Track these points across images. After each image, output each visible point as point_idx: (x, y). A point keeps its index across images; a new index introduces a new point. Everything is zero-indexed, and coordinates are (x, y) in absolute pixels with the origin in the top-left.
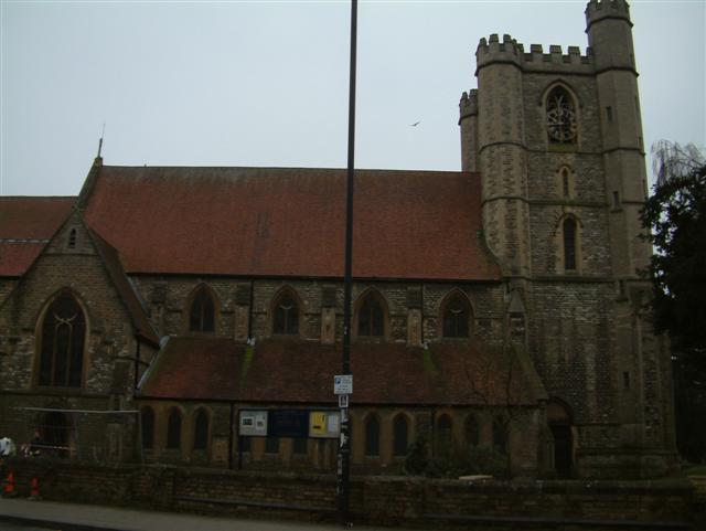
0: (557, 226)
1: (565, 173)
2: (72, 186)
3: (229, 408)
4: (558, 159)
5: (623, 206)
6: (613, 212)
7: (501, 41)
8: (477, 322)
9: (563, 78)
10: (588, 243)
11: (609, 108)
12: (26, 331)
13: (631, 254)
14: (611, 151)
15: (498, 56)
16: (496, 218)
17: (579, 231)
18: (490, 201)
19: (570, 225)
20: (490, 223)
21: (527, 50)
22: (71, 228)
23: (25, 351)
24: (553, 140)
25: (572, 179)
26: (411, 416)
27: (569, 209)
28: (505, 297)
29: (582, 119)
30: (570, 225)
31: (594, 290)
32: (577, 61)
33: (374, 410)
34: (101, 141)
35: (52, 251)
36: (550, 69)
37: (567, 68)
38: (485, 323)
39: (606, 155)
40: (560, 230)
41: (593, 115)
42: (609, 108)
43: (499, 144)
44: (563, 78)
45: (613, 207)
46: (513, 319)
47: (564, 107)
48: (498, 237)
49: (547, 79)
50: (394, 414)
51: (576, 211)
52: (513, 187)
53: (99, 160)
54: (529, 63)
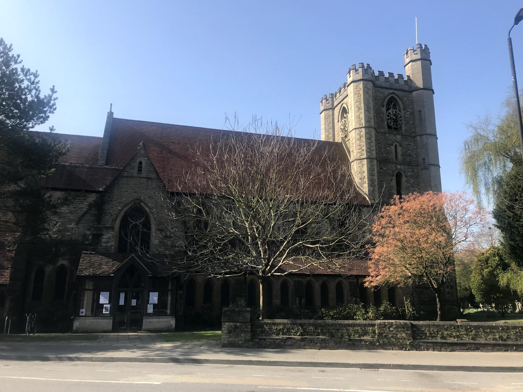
1: (396, 146)
2: (97, 130)
4: (392, 137)
9: (395, 92)
10: (409, 186)
12: (107, 228)
21: (377, 74)
22: (138, 161)
23: (108, 242)
24: (389, 127)
25: (399, 149)
27: (399, 167)
29: (405, 116)
32: (382, 79)
34: (111, 104)
35: (126, 174)
36: (388, 86)
37: (396, 86)
41: (410, 114)
44: (395, 92)
47: (394, 108)
49: (387, 92)
52: (373, 152)
53: (111, 114)
54: (377, 81)
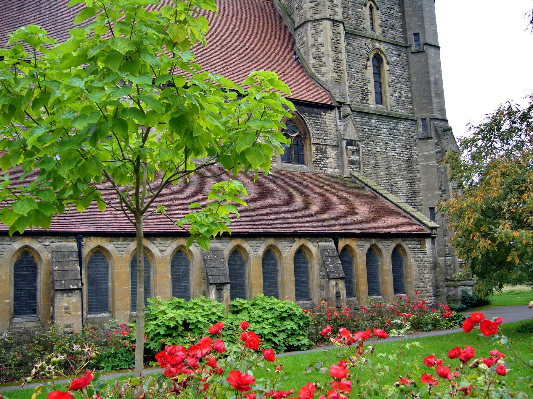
0: (368, 60)
3: (332, 244)
5: (425, 48)
8: (313, 148)
13: (433, 95)
16: (320, 40)
17: (386, 67)
18: (314, 21)
19: (378, 59)
20: (313, 45)
25: (377, 14)
26: (313, 247)
27: (377, 45)
28: (339, 123)
30: (378, 59)
31: (401, 126)
33: (271, 241)
38: (321, 150)
40: (370, 63)
45: (414, 48)
46: (349, 147)
48: (324, 60)
50: (296, 245)
51: (383, 47)
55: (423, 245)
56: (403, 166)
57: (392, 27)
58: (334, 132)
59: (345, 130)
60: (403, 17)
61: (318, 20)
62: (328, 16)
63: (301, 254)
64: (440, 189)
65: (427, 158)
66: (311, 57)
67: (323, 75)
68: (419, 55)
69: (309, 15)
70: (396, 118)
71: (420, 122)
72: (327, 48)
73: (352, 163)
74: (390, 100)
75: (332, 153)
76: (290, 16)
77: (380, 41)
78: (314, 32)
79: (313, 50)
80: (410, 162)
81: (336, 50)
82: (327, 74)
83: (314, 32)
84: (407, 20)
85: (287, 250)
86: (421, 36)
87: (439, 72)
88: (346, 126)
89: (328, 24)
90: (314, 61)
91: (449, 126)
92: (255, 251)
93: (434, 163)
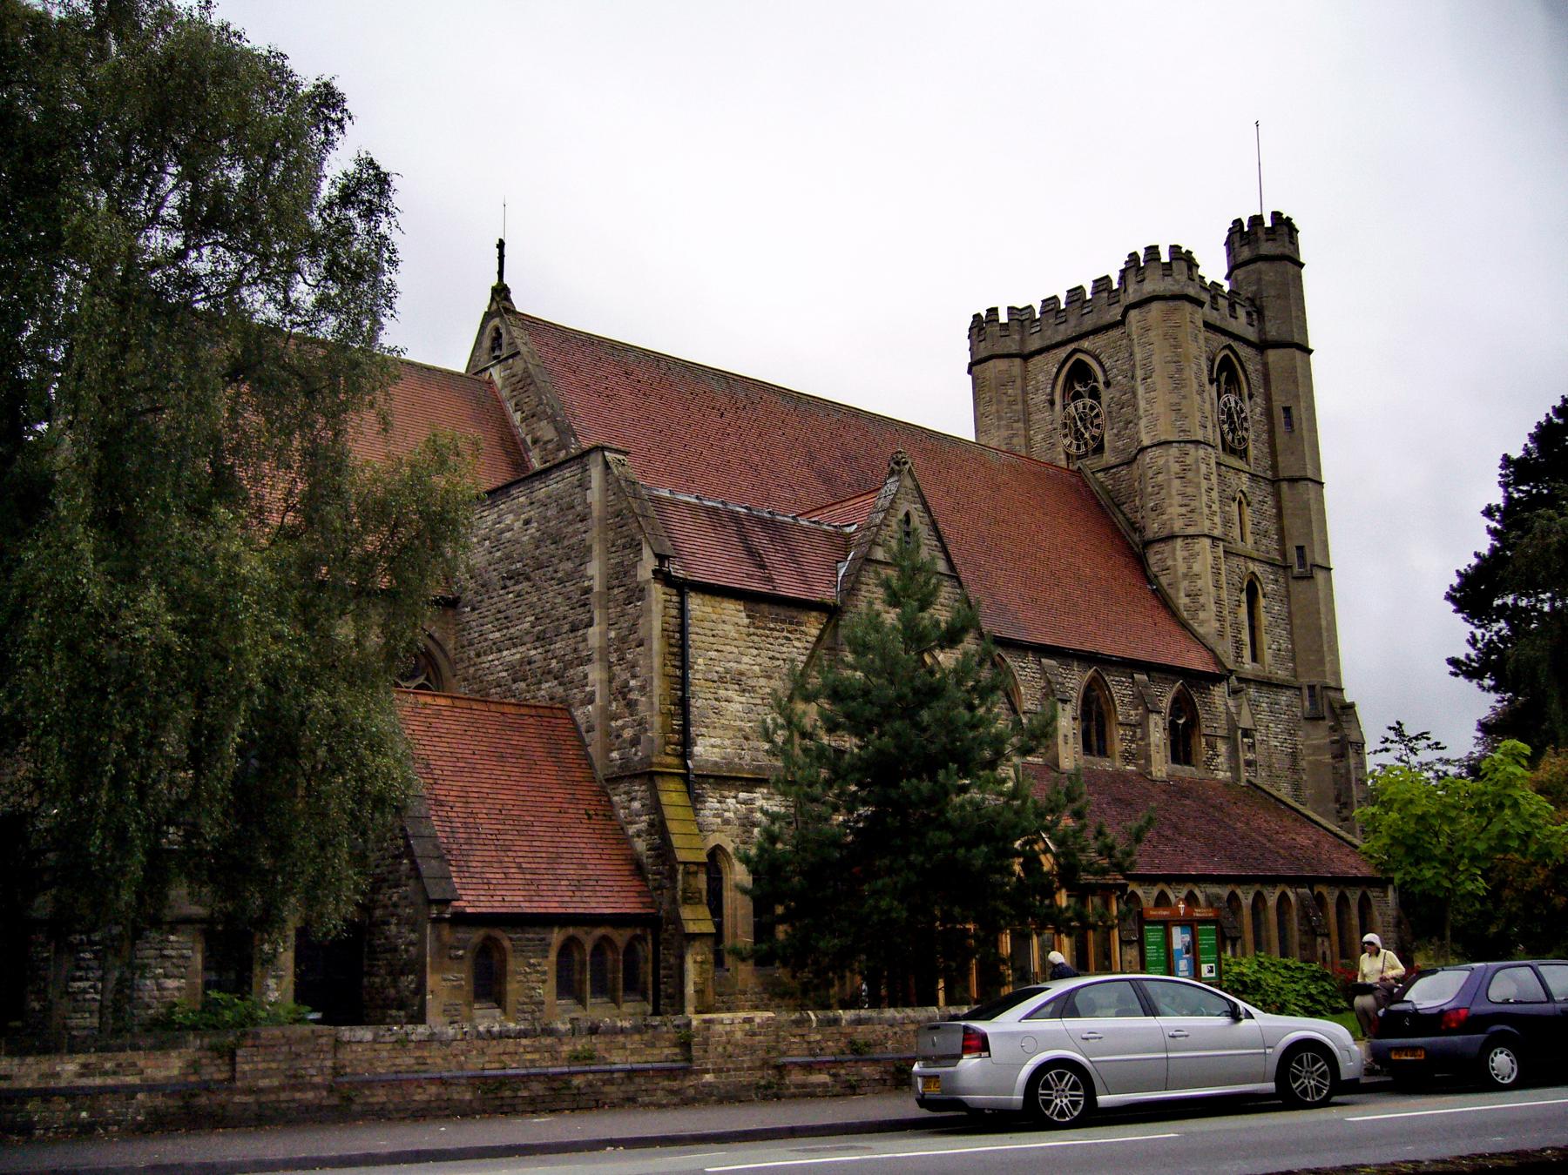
6: (1296, 578)
7: (1165, 258)
9: (1234, 344)
11: (1287, 410)
14: (1293, 480)
15: (1506, 458)
16: (1196, 568)
17: (1262, 602)
18: (1186, 537)
19: (1252, 591)
20: (1185, 576)
25: (1247, 511)
30: (1252, 591)
31: (1284, 698)
34: (501, 245)
39: (1284, 485)
42: (1287, 410)
43: (1197, 442)
45: (1296, 570)
48: (1202, 600)
55: (1385, 892)
56: (1287, 761)
57: (1266, 534)
58: (1224, 716)
59: (1239, 714)
60: (1280, 515)
61: (1193, 537)
62: (1206, 532)
63: (1259, 898)
64: (1337, 800)
65: (1317, 749)
66: (1182, 594)
67: (1201, 623)
68: (1305, 583)
69: (1178, 526)
70: (1277, 686)
71: (1306, 692)
72: (1206, 582)
73: (1249, 763)
74: (1267, 655)
75: (1222, 748)
76: (1118, 506)
77: (1253, 559)
78: (1186, 554)
79: (1186, 583)
80: (1294, 756)
81: (1218, 587)
82: (1207, 624)
83: (1186, 554)
84: (1286, 522)
85: (1354, 896)
86: (1307, 551)
87: (1331, 611)
88: (1239, 707)
89: (1207, 542)
90: (1187, 600)
91: (1348, 700)
92: (1246, 897)
93: (1327, 758)
